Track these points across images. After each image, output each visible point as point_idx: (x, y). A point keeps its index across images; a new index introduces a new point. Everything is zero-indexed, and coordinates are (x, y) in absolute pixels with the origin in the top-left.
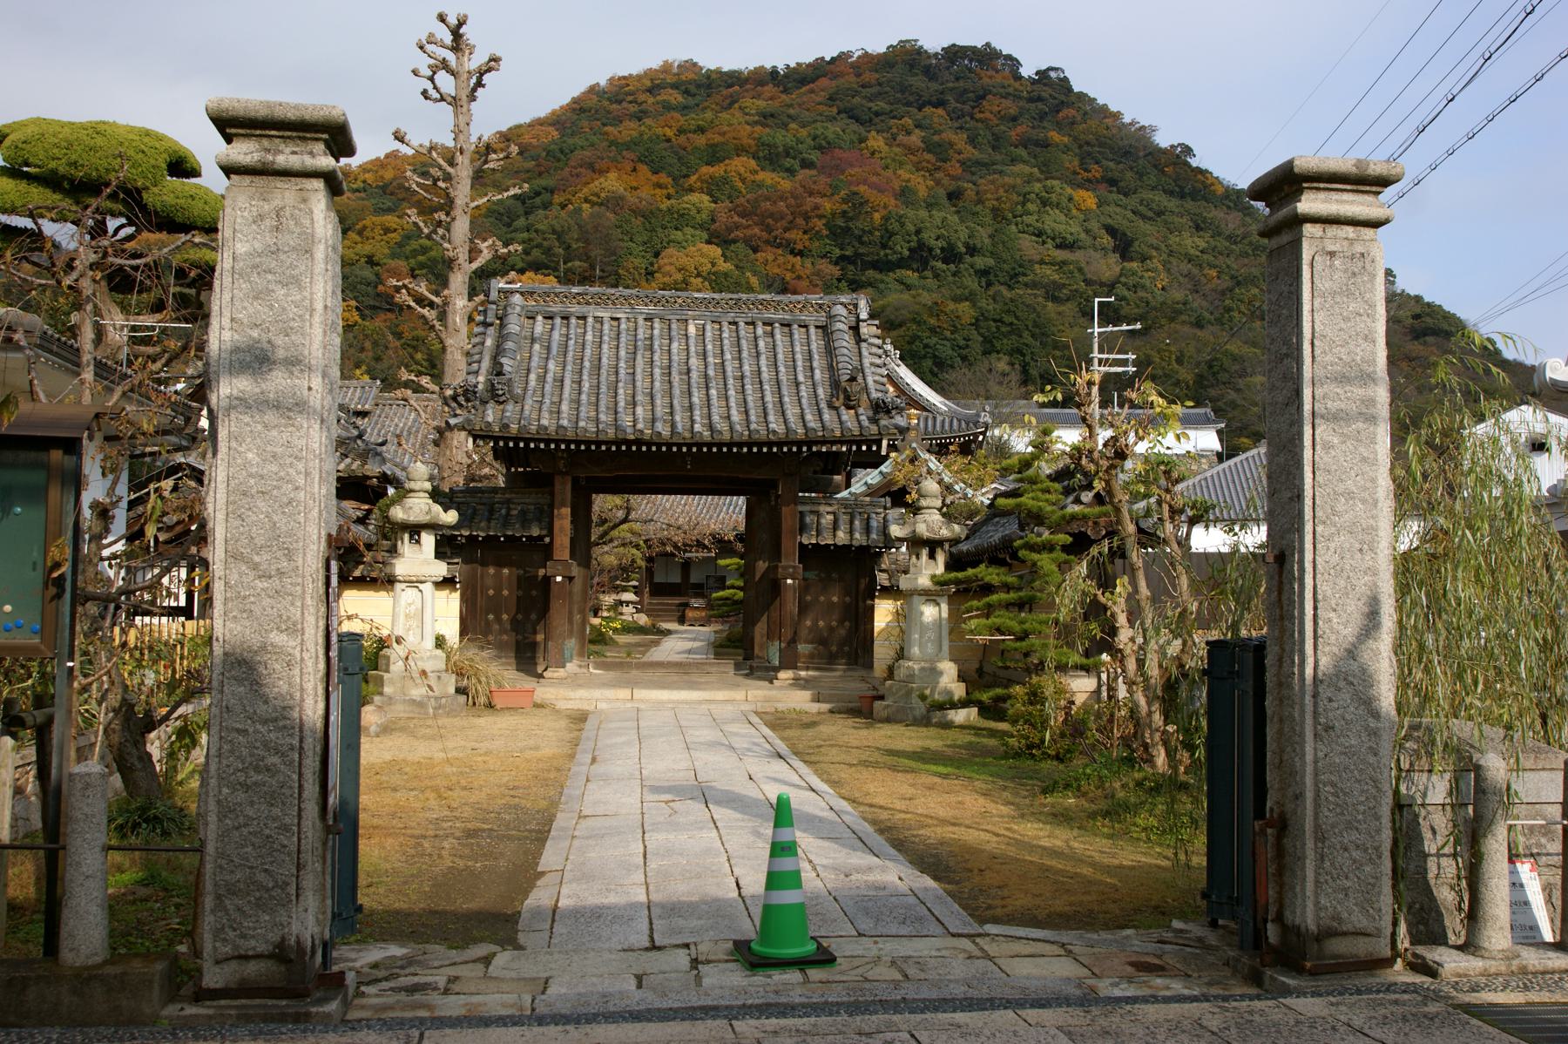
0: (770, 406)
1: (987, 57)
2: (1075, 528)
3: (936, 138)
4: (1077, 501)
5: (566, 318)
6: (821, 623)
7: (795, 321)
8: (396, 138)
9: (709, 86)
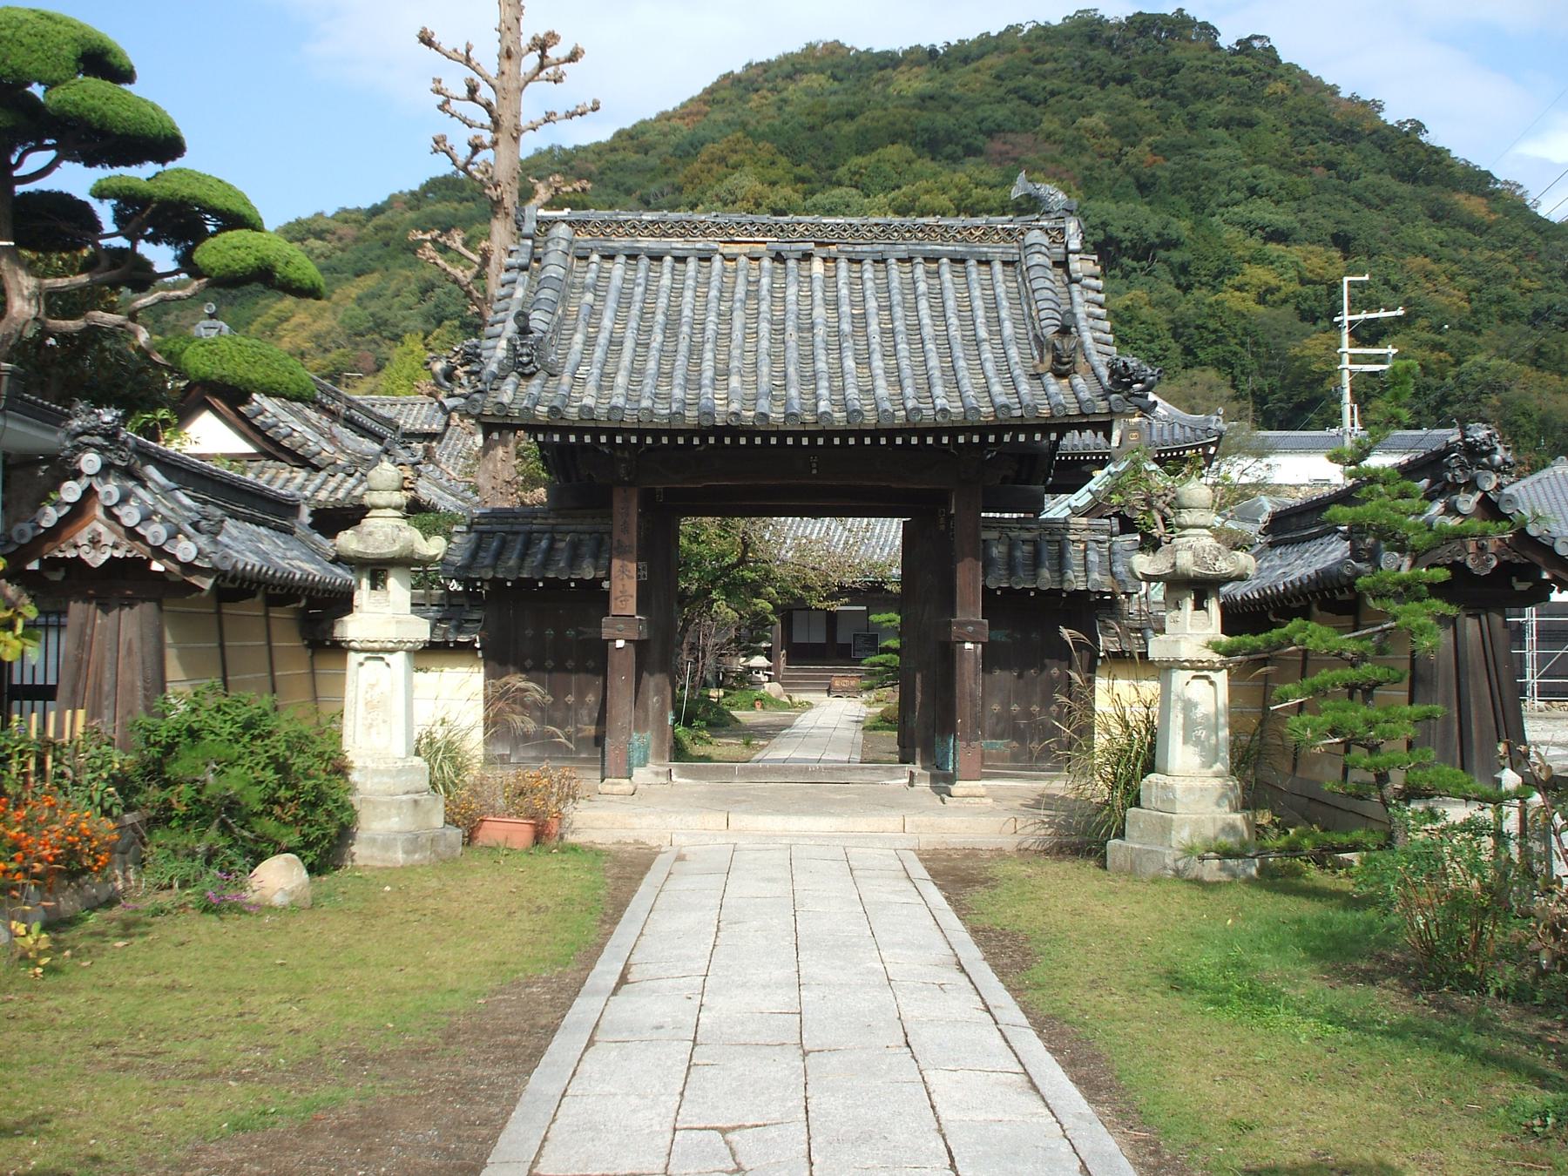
0: (936, 373)
1: (1180, 25)
2: (1444, 554)
3: (1123, 119)
4: (1451, 510)
5: (632, 257)
6: (1015, 708)
7: (972, 254)
8: (422, 40)
9: (860, 70)
